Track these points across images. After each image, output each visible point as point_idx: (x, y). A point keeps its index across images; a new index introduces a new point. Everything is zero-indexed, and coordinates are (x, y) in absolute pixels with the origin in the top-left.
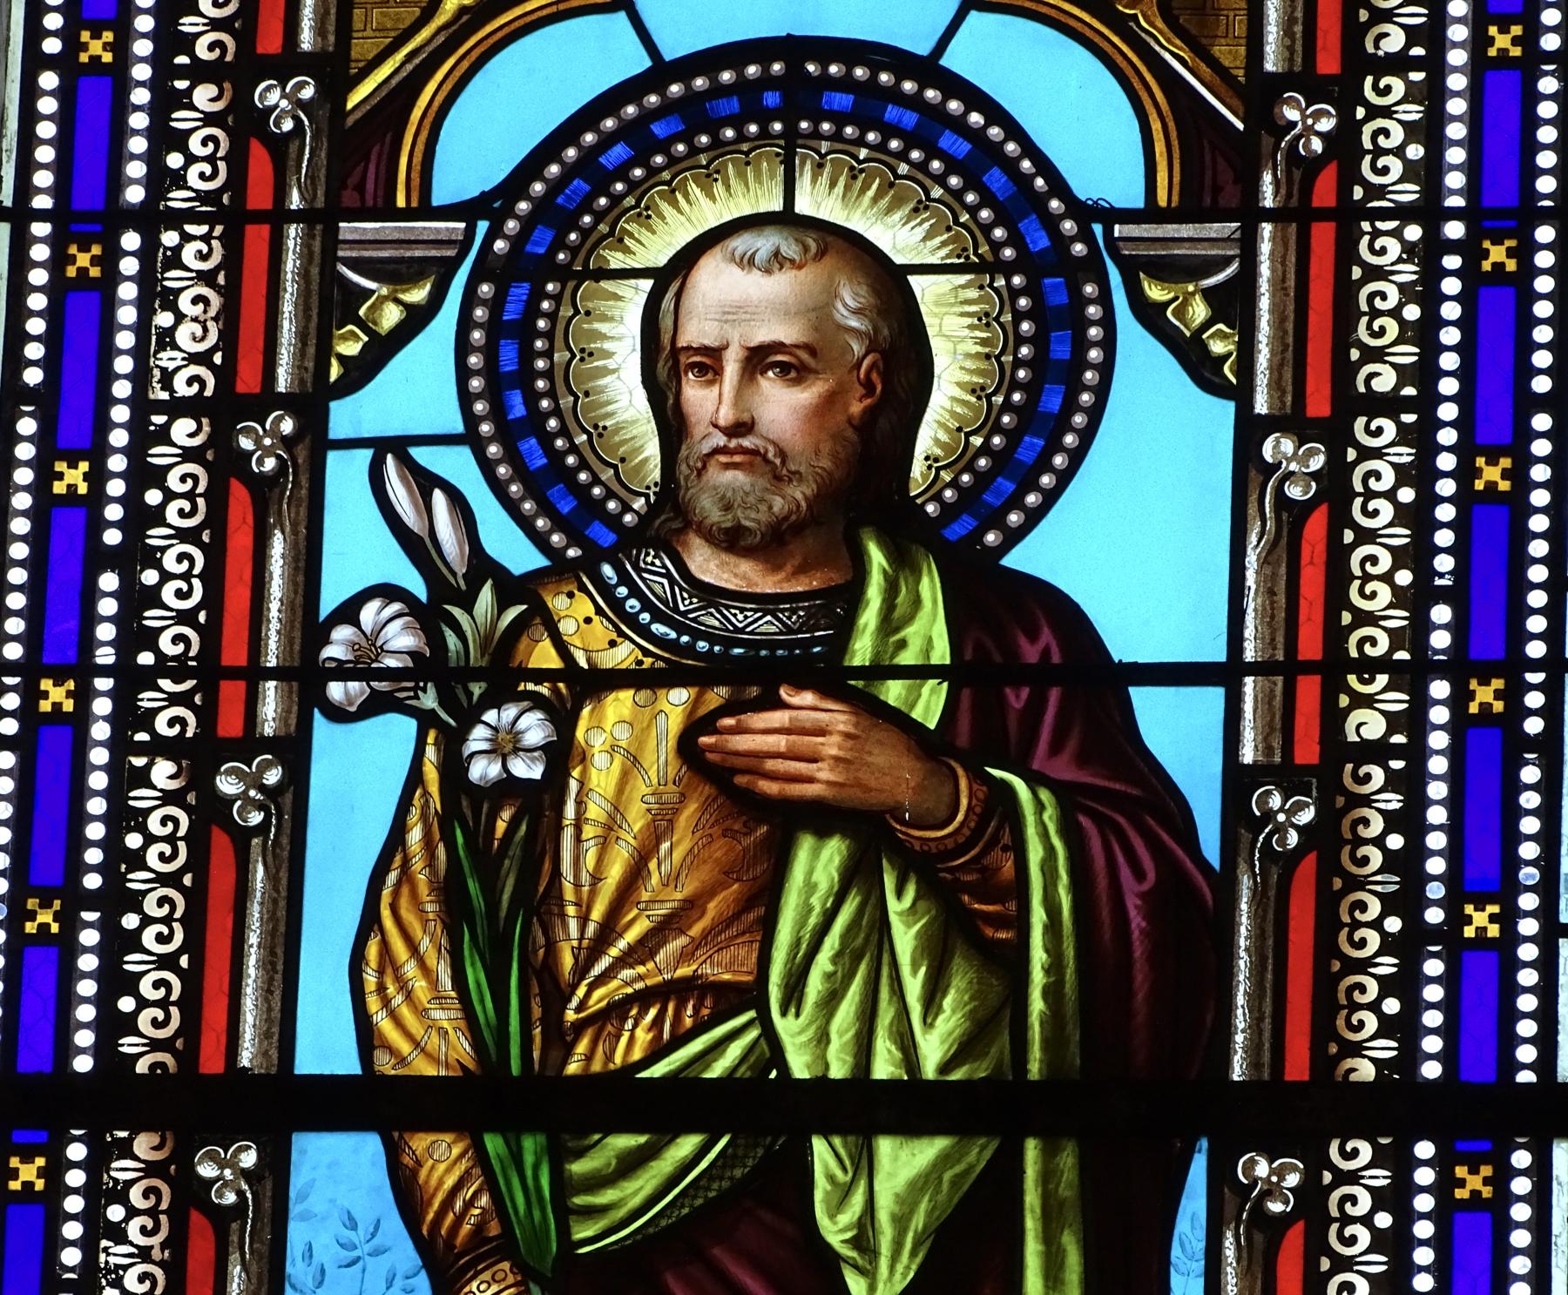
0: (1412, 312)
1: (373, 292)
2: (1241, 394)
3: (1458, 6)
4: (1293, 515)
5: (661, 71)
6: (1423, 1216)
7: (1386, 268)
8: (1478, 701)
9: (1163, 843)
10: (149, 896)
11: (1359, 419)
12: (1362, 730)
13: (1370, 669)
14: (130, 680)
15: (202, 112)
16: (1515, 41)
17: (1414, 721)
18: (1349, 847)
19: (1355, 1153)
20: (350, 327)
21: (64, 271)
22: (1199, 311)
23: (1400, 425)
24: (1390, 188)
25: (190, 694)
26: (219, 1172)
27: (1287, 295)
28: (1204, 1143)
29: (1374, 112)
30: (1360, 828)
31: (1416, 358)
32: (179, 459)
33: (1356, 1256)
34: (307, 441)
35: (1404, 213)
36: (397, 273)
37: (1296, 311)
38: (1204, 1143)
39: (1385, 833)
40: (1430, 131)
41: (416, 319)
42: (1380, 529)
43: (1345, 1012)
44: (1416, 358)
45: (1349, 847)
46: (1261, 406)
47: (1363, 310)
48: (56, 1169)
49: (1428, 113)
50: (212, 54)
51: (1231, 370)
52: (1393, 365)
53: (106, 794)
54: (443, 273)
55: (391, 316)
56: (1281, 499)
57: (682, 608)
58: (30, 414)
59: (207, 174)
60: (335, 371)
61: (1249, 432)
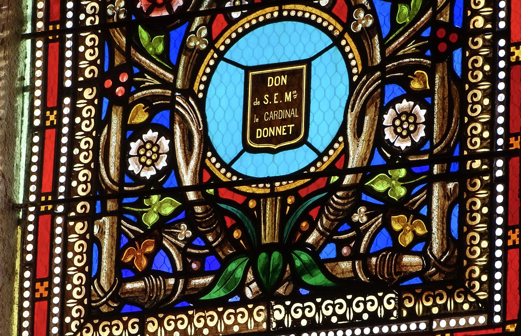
7: (78, 272)
9: (134, 211)
11: (96, 77)
13: (93, 29)
16: (52, 113)
18: (81, 317)
19: (133, 327)
23: (84, 76)
24: (351, 309)
28: (124, 215)
29: (251, 312)
31: (78, 102)
34: (329, 282)
38: (124, 215)
39: (239, 324)
40: (77, 57)
42: (83, 169)
43: (82, 317)
44: (76, 134)
45: (81, 317)
47: (89, 184)
50: (91, 43)
52: (85, 99)
53: (497, 193)
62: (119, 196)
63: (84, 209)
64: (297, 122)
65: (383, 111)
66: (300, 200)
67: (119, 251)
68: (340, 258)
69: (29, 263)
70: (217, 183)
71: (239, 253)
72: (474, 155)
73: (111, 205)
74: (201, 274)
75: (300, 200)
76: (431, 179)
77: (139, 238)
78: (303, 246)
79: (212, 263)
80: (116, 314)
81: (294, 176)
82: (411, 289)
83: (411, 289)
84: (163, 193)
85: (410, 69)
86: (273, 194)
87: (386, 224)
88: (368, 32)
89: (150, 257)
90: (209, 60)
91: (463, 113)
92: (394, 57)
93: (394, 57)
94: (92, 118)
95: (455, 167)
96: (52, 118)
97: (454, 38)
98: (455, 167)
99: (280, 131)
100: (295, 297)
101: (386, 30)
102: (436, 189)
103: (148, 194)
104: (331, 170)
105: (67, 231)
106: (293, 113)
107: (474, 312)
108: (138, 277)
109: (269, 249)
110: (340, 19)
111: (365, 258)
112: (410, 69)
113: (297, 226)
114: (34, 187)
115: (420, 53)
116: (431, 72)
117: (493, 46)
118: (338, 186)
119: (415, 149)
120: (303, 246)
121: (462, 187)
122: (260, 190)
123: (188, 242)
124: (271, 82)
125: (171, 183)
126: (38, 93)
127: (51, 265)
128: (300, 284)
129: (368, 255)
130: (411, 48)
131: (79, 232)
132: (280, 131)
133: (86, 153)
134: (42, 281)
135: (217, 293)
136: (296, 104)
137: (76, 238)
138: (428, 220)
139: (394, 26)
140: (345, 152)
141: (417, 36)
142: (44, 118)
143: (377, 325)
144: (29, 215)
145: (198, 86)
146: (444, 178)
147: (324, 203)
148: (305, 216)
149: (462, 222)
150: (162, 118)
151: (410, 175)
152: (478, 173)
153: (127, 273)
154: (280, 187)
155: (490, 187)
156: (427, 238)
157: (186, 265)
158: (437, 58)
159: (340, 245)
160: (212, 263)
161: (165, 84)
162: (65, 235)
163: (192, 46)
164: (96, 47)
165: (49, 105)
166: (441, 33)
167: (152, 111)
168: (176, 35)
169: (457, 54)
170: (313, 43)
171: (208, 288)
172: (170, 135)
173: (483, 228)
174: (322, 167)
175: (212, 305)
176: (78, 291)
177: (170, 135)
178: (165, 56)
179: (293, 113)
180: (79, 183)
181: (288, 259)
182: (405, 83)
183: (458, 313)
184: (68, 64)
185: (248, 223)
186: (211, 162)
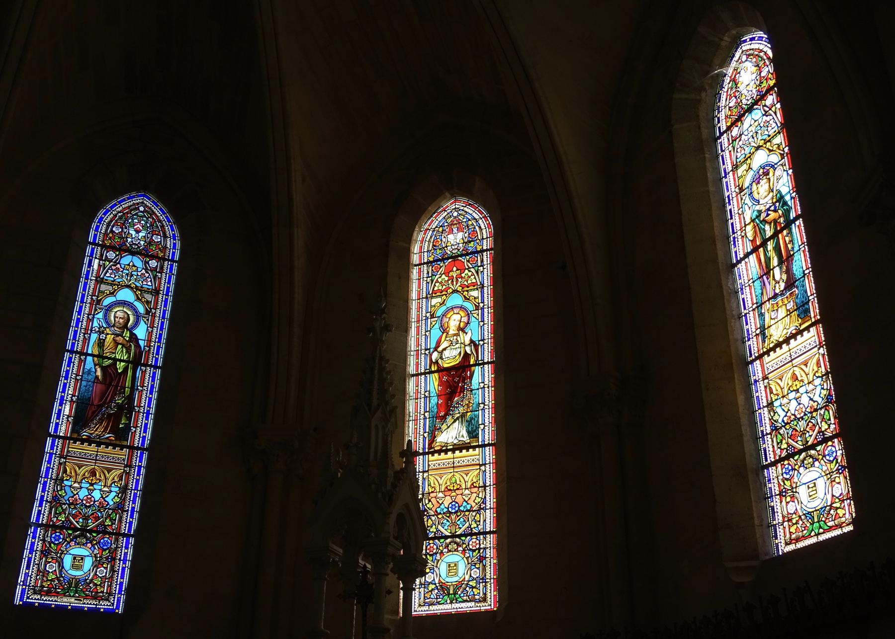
14: (81, 329)
36: (100, 309)
54: (437, 321)
62: (425, 584)
64: (456, 572)
65: (471, 570)
66: (457, 586)
67: (425, 594)
68: (464, 596)
70: (442, 583)
71: (446, 595)
72: (487, 579)
73: (423, 586)
74: (440, 598)
75: (457, 586)
76: (480, 583)
77: (428, 592)
78: (457, 594)
79: (441, 597)
80: (424, 605)
81: (456, 582)
82: (477, 602)
83: (477, 602)
84: (433, 584)
85: (476, 564)
86: (452, 585)
87: (472, 590)
88: (468, 557)
89: (430, 596)
90: (440, 561)
91: (485, 571)
92: (473, 561)
93: (473, 561)
95: (484, 581)
97: (484, 559)
98: (484, 581)
99: (453, 574)
100: (456, 603)
101: (471, 556)
102: (481, 584)
103: (429, 584)
104: (462, 581)
106: (455, 571)
107: (488, 606)
108: (428, 599)
109: (452, 594)
111: (469, 596)
112: (476, 564)
113: (456, 591)
115: (478, 561)
116: (108, 564)
117: (490, 560)
118: (464, 584)
119: (477, 578)
120: (457, 594)
121: (486, 584)
122: (450, 584)
123: (437, 593)
124: (77, 558)
125: (434, 582)
128: (457, 600)
129: (469, 596)
130: (476, 560)
132: (453, 574)
135: (442, 602)
136: (456, 569)
138: (480, 590)
139: (473, 556)
140: (465, 578)
141: (477, 558)
145: (438, 566)
146: (482, 582)
147: (461, 586)
148: (458, 589)
149: (486, 590)
150: (432, 571)
151: (477, 582)
152: (488, 582)
153: (426, 598)
154: (453, 583)
155: (491, 584)
156: (480, 593)
157: (437, 597)
158: (480, 562)
159: (464, 594)
160: (441, 597)
161: (432, 565)
163: (827, 510)
166: (481, 558)
167: (430, 570)
168: (434, 557)
169: (484, 561)
171: (440, 601)
172: (433, 573)
173: (490, 591)
174: (460, 580)
175: (441, 604)
177: (433, 573)
178: (432, 560)
179: (455, 571)
181: (455, 596)
182: (475, 566)
183: (485, 606)
185: (448, 590)
186: (441, 579)
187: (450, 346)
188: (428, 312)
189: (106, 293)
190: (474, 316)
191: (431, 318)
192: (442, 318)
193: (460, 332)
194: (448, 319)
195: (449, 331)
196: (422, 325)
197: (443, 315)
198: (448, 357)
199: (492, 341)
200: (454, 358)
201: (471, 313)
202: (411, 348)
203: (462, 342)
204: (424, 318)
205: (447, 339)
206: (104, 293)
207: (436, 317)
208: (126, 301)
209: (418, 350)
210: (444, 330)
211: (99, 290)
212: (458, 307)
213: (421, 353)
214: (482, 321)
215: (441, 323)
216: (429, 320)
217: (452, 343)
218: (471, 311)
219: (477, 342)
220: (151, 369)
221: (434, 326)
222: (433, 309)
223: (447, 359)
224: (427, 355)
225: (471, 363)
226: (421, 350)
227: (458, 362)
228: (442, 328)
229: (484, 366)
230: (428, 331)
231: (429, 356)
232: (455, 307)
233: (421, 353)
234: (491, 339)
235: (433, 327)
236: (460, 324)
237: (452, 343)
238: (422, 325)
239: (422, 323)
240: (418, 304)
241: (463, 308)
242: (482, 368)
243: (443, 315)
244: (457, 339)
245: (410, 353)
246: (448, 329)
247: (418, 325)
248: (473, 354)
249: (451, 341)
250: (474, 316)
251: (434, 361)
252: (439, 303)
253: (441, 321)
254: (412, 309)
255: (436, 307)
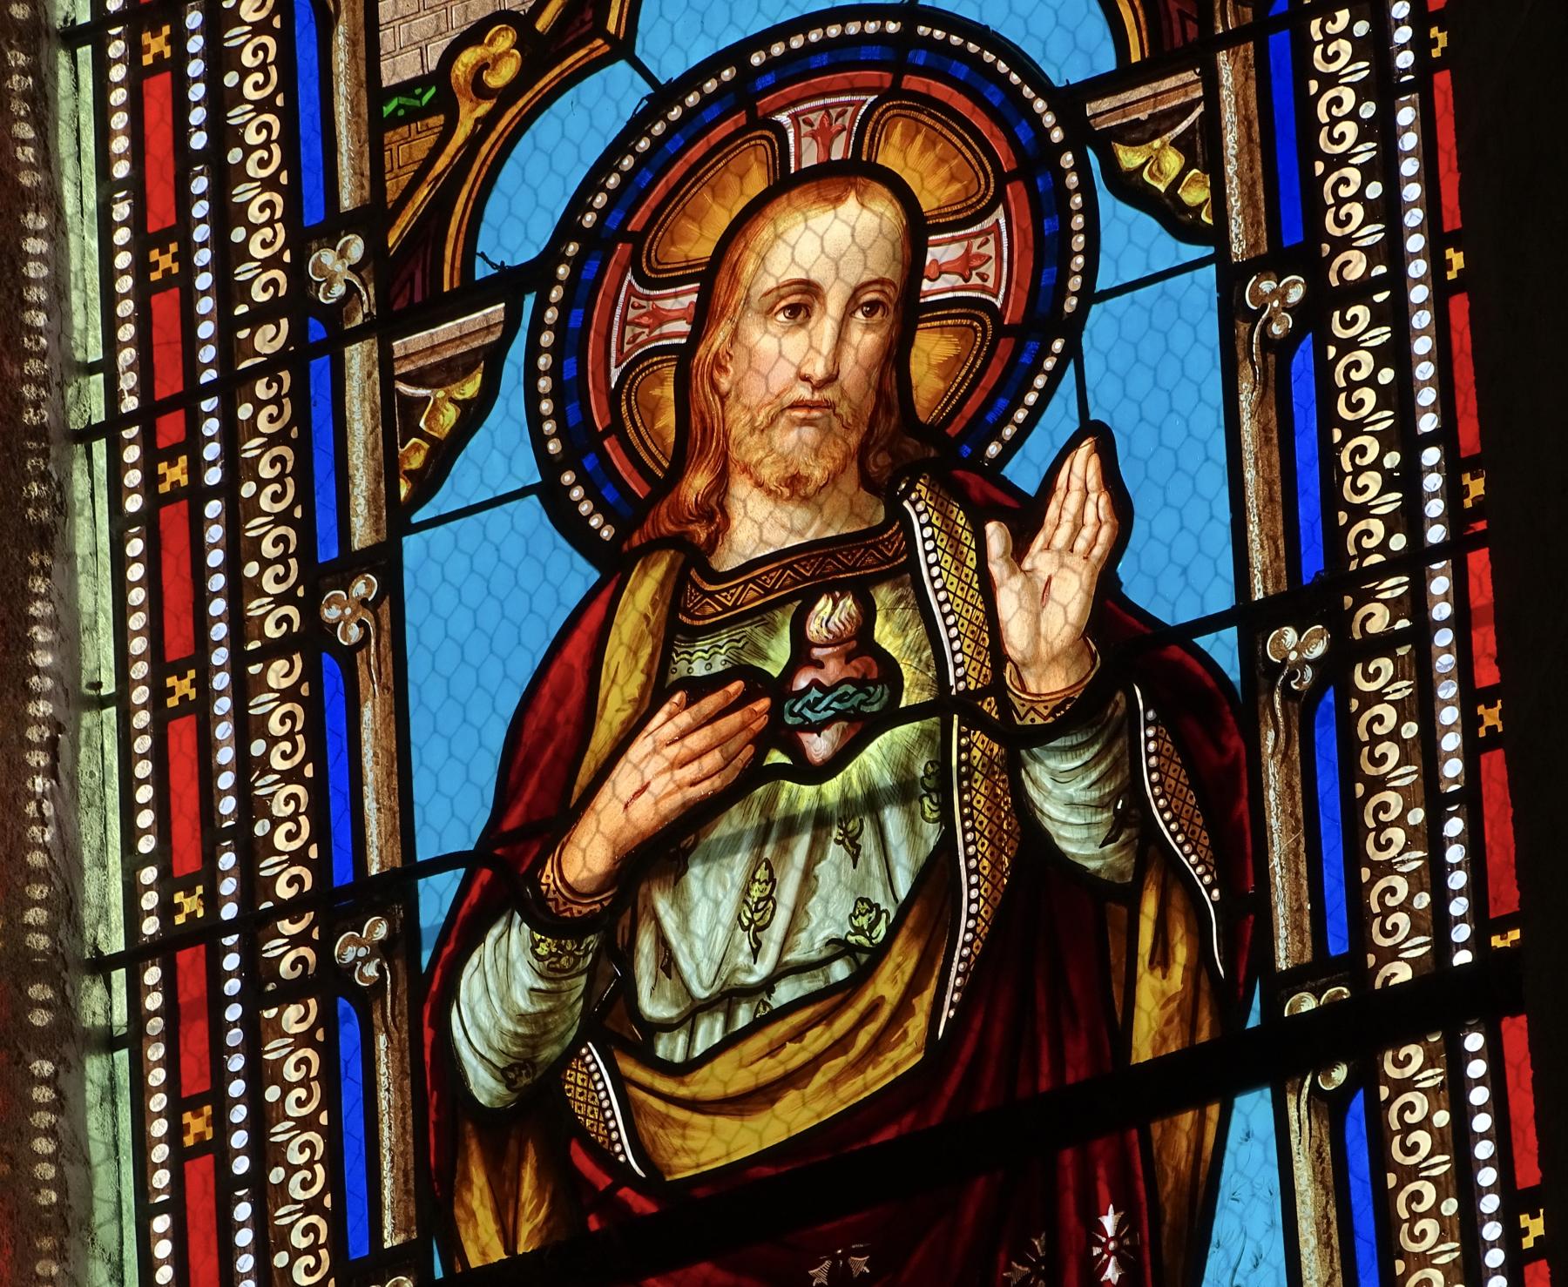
0: (1374, 190)
1: (427, 399)
2: (1217, 235)
3: (1400, 10)
4: (1281, 350)
5: (663, 95)
6: (1476, 1055)
8: (1471, 496)
10: (291, 1145)
12: (1345, 272)
15: (265, 355)
17: (1417, 601)
20: (414, 440)
21: (182, 1142)
22: (1173, 162)
25: (307, 931)
26: (340, 612)
27: (1259, 209)
30: (1407, 1113)
32: (273, 606)
33: (1389, 773)
35: (1394, 565)
36: (447, 372)
37: (1279, 425)
41: (474, 414)
46: (1238, 249)
48: (179, 38)
49: (1464, 1249)
50: (305, 1240)
51: (1207, 215)
54: (493, 358)
55: (450, 416)
56: (1267, 341)
57: (730, 604)
58: (137, 536)
59: (261, 82)
60: (404, 489)
61: (1231, 279)
63: (279, 465)
69: (135, 519)
94: (314, 1079)
96: (166, 262)
105: (243, 689)
110: (1127, 291)
114: (133, 551)
126: (156, 1052)
127: (202, 622)
131: (279, 683)
133: (307, 1174)
134: (202, 1146)
137: (256, 268)
142: (167, 910)
143: (1249, 1084)
144: (138, 787)
162: (253, 1048)
164: (278, 221)
165: (171, 655)
170: (1020, 17)
176: (304, 1180)
180: (296, 1254)
184: (218, 607)
187: (755, 775)
188: (333, 227)
189: (479, 89)
190: (1131, 189)
191: (386, 327)
192: (581, 295)
193: (920, 511)
194: (934, 288)
195: (715, 512)
196: (236, 468)
197: (598, 244)
198: (728, 997)
199: (1482, 594)
200: (835, 998)
201: (1081, 134)
202: (67, 907)
203: (965, 673)
204: (269, 339)
205: (700, 662)
206: (447, 105)
207: (472, 296)
208: (579, 203)
209: (208, 932)
210: (628, 513)
211: (373, 89)
212: (841, 54)
213: (256, 970)
214: (1275, 262)
215: (569, 392)
216: (358, 357)
217: (779, 733)
218: (1069, 101)
219: (1223, 648)
220: (1456, 1060)
221: (445, 453)
222: (409, 148)
223: (710, 1032)
224: (365, 1000)
225: (1143, 1050)
226: (254, 927)
227: (905, 1055)
228: (599, 482)
229: (1367, 1076)
230: (349, 565)
231: (389, 1006)
232: (794, 68)
233: (256, 970)
234: (1453, 550)
235: (429, 481)
236: (896, 355)
237: (779, 733)
238: (236, 468)
239: (232, 435)
240: (158, 89)
241: (941, 62)
242: (1331, 1107)
243: (598, 244)
244: (860, 641)
245: (65, 1007)
246: (697, 483)
247: (175, 474)
248: (1175, 873)
249: (757, 682)
250: (1131, 189)
251: (484, 1085)
252: (504, 40)
253: (571, 343)
254: (52, 201)
255: (470, 114)
